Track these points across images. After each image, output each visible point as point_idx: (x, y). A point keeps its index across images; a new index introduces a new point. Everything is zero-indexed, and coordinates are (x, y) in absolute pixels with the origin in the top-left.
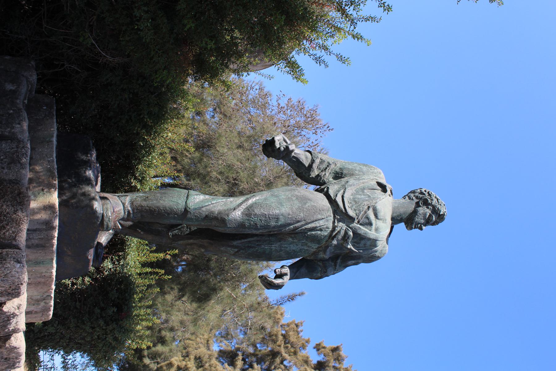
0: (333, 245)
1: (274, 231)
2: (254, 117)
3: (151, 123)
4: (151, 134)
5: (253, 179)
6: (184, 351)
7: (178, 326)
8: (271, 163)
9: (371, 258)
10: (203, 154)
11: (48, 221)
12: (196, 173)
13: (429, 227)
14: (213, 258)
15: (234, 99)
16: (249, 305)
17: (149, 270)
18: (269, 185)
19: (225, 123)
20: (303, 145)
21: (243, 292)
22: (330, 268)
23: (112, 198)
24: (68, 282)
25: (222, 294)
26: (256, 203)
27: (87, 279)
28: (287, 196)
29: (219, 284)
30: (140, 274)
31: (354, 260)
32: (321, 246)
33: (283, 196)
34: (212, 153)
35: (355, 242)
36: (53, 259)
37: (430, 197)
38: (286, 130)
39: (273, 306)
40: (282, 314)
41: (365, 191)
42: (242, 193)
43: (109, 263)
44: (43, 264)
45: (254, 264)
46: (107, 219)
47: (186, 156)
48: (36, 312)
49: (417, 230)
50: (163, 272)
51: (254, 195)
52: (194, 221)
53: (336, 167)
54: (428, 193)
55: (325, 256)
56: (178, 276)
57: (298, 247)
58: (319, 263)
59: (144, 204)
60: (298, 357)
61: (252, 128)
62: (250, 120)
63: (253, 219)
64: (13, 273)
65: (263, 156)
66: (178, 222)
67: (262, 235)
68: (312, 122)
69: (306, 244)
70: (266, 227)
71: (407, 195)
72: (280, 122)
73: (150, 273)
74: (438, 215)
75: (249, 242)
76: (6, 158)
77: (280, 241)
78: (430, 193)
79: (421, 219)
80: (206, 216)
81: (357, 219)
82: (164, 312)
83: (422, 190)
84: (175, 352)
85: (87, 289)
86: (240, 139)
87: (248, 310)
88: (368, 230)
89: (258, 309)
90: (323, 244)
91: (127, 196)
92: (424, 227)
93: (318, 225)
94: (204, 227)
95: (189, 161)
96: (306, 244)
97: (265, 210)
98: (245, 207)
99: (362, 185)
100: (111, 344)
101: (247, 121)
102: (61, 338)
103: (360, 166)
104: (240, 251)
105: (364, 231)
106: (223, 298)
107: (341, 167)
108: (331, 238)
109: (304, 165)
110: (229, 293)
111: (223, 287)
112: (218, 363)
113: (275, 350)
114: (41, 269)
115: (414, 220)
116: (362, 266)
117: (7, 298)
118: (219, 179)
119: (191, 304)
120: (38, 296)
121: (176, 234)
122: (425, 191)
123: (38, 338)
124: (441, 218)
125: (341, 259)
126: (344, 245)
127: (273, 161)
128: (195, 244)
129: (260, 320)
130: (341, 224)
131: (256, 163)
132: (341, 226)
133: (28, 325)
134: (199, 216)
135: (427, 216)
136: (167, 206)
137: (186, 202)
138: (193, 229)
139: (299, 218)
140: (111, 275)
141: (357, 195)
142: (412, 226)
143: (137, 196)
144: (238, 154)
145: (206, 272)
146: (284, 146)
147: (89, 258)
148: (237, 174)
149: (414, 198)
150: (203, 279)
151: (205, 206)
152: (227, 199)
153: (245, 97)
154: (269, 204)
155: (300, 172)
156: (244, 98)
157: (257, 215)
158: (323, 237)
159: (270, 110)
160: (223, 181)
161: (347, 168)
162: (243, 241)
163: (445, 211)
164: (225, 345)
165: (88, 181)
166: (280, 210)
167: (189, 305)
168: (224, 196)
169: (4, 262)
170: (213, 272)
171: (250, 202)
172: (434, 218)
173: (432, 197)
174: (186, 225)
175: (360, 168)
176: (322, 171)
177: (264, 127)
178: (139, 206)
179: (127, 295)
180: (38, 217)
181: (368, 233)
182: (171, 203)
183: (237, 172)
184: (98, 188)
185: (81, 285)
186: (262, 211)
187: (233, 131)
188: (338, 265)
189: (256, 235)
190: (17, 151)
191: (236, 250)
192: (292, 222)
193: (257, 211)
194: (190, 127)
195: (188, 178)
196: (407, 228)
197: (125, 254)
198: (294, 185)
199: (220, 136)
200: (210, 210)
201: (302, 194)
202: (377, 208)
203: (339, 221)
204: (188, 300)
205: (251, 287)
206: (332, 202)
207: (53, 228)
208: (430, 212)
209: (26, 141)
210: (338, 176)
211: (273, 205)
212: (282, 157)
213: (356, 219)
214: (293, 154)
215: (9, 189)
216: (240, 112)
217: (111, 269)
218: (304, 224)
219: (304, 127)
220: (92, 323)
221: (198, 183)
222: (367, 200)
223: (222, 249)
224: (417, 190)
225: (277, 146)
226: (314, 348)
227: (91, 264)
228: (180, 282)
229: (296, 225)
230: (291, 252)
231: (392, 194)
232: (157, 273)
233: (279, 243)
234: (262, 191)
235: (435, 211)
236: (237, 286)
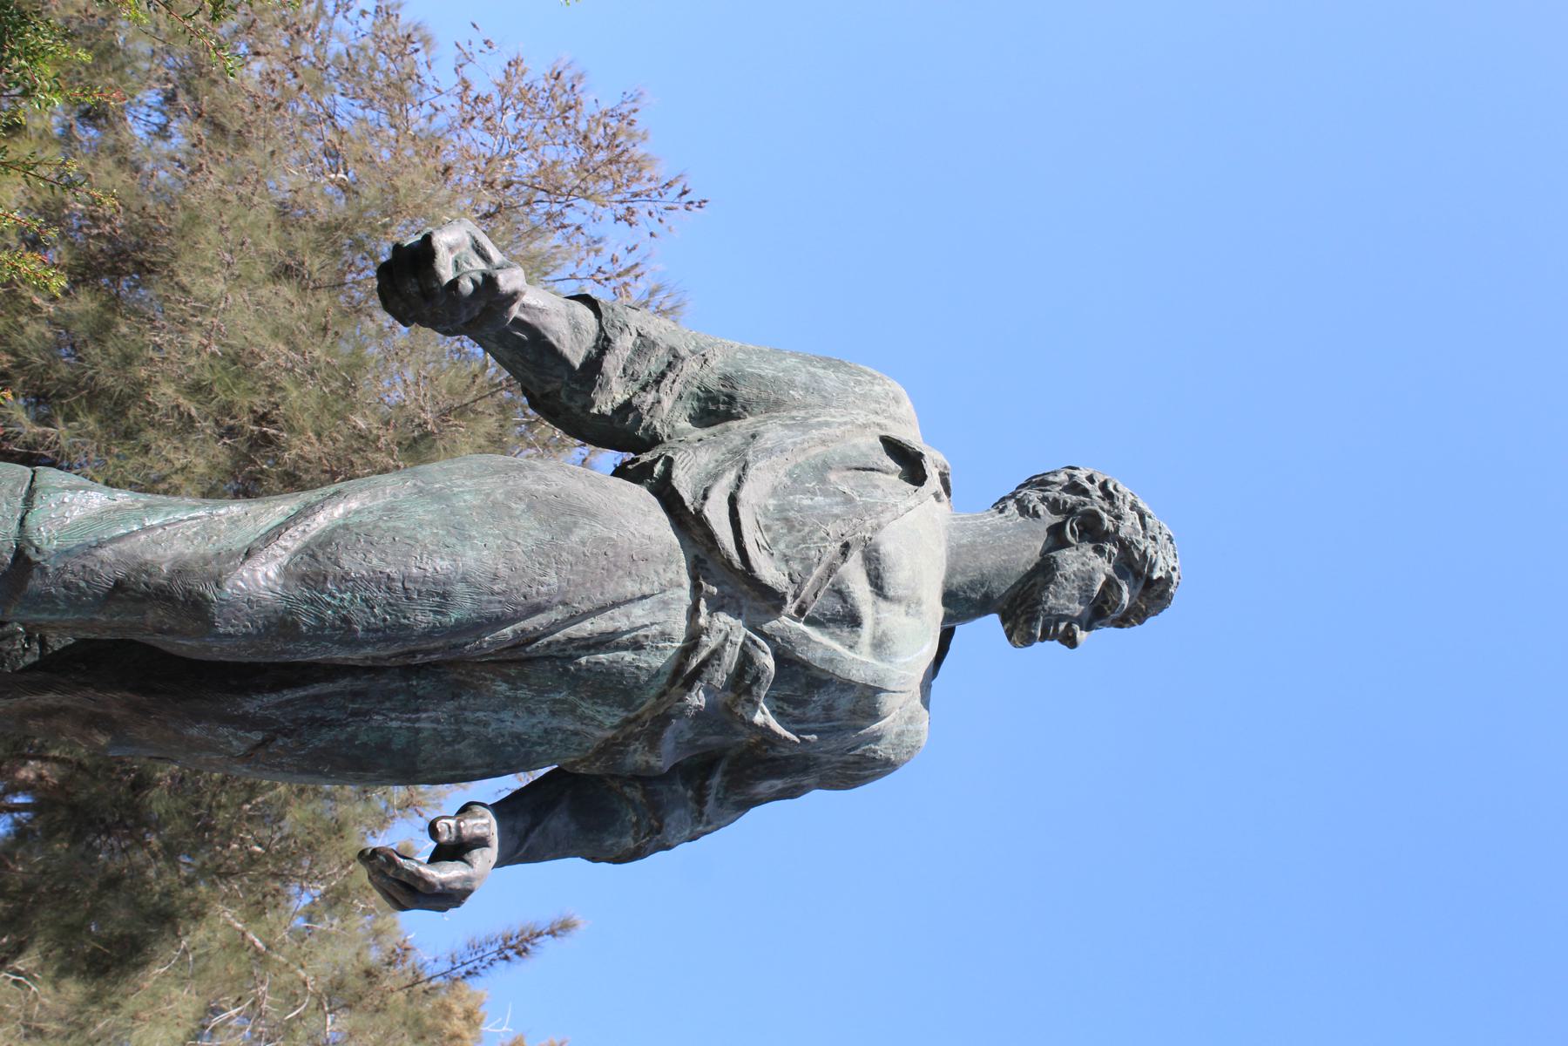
0: (690, 713)
1: (428, 652)
2: (351, 141)
5: (345, 419)
8: (429, 349)
10: (113, 304)
12: (80, 390)
14: (158, 775)
15: (257, 54)
16: (325, 980)
19: (217, 162)
20: (570, 268)
21: (300, 922)
22: (679, 813)
25: (201, 934)
26: (346, 527)
28: (488, 495)
29: (187, 893)
31: (780, 774)
32: (638, 717)
33: (467, 497)
34: (158, 296)
35: (785, 699)
37: (1112, 504)
38: (498, 199)
39: (433, 983)
40: (469, 1016)
41: (833, 477)
42: (292, 481)
45: (349, 798)
47: (35, 308)
49: (1055, 646)
52: (62, 606)
53: (706, 370)
54: (1104, 486)
55: (653, 761)
57: (535, 721)
58: (627, 790)
61: (344, 188)
62: (331, 153)
63: (334, 597)
67: (373, 669)
68: (614, 168)
69: (573, 710)
70: (394, 632)
71: (1013, 495)
72: (470, 164)
74: (1142, 583)
75: (318, 698)
77: (455, 696)
78: (1111, 487)
79: (1070, 599)
80: (119, 585)
81: (796, 596)
83: (1076, 472)
86: (284, 235)
87: (320, 1006)
88: (843, 644)
89: (367, 1001)
90: (642, 709)
92: (1081, 636)
93: (623, 624)
94: (107, 636)
95: (49, 335)
96: (573, 710)
97: (389, 559)
101: (321, 156)
103: (812, 369)
104: (273, 740)
105: (827, 648)
106: (207, 954)
107: (730, 370)
108: (680, 681)
109: (563, 360)
110: (236, 929)
111: (204, 903)
115: (1039, 602)
116: (817, 799)
118: (189, 415)
119: (57, 988)
122: (1091, 479)
125: (725, 774)
126: (739, 710)
127: (433, 343)
130: (724, 620)
131: (363, 347)
132: (724, 629)
134: (83, 584)
135: (1098, 588)
137: (23, 519)
138: (57, 643)
139: (538, 594)
142: (1030, 627)
144: (279, 304)
145: (130, 836)
146: (474, 275)
148: (270, 394)
149: (1042, 508)
151: (113, 540)
152: (215, 507)
153: (311, 48)
154: (408, 533)
155: (548, 388)
156: (305, 50)
157: (353, 580)
158: (644, 678)
159: (426, 109)
160: (208, 426)
161: (752, 374)
162: (288, 694)
163: (1172, 563)
166: (454, 557)
167: (49, 989)
168: (211, 493)
170: (159, 837)
171: (321, 521)
172: (1126, 597)
173: (1119, 503)
174: (23, 625)
175: (813, 375)
176: (643, 389)
177: (398, 183)
183: (273, 388)
186: (375, 561)
187: (256, 199)
188: (711, 800)
189: (333, 671)
191: (257, 736)
192: (509, 610)
193: (352, 563)
194: (43, 179)
195: (43, 410)
196: (1009, 638)
198: (530, 445)
199: (194, 219)
200: (135, 557)
201: (554, 489)
202: (882, 549)
203: (716, 606)
204: (42, 969)
205: (336, 899)
208: (1109, 568)
211: (425, 534)
212: (466, 324)
213: (789, 599)
214: (515, 311)
216: (288, 116)
218: (563, 621)
219: (576, 191)
221: (92, 435)
222: (837, 516)
223: (194, 732)
224: (1055, 473)
225: (442, 271)
229: (529, 624)
230: (505, 744)
233: (451, 705)
234: (385, 470)
235: (1130, 566)
236: (269, 899)
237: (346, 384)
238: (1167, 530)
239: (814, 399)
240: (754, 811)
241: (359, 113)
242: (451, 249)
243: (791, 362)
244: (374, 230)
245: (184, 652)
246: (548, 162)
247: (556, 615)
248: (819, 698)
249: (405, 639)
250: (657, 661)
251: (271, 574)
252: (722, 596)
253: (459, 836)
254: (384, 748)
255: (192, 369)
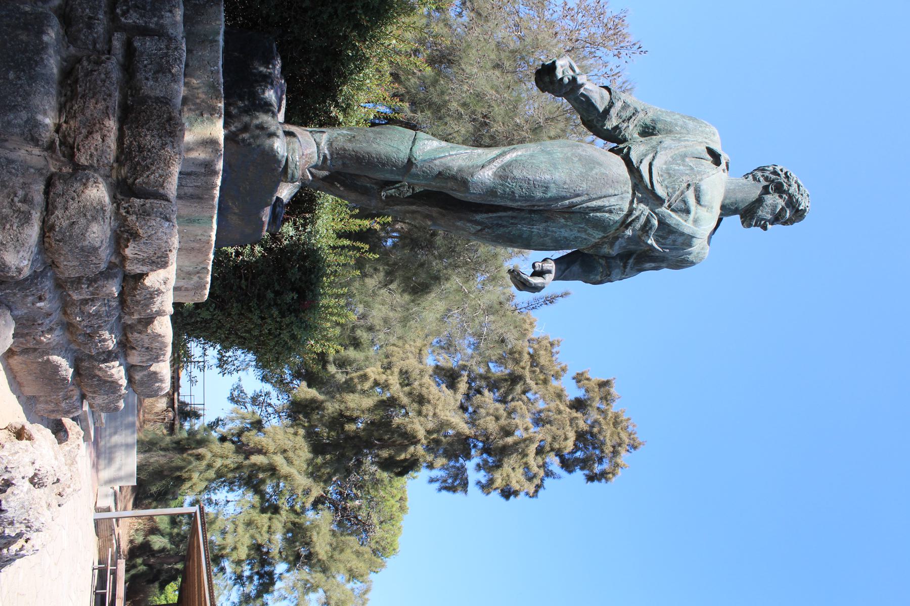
1: (539, 206)
3: (368, 22)
4: (365, 40)
5: (513, 119)
6: (385, 360)
7: (380, 325)
9: (681, 263)
10: (439, 73)
11: (209, 162)
12: (426, 102)
13: (778, 227)
17: (347, 242)
18: (536, 131)
22: (617, 270)
23: (301, 134)
24: (231, 250)
25: (448, 285)
27: (257, 248)
30: (334, 248)
31: (654, 262)
35: (660, 236)
36: (212, 217)
37: (788, 180)
40: (531, 324)
41: (687, 160)
42: (493, 143)
43: (291, 229)
44: (199, 223)
46: (293, 166)
47: (414, 73)
48: (187, 289)
49: (759, 229)
50: (367, 247)
51: (514, 148)
53: (646, 117)
54: (786, 173)
55: (611, 251)
56: (386, 253)
59: (349, 146)
60: (549, 388)
61: (520, 38)
62: (517, 25)
64: (160, 234)
65: (531, 84)
66: (397, 177)
67: (520, 210)
68: (615, 37)
69: (585, 231)
70: (528, 198)
71: (751, 173)
73: (348, 247)
75: (500, 217)
76: (151, 64)
77: (546, 222)
78: (788, 174)
79: (767, 213)
80: (440, 173)
81: (668, 201)
82: (361, 303)
84: (373, 361)
85: (256, 262)
91: (324, 132)
92: (769, 226)
93: (607, 204)
96: (585, 231)
98: (500, 165)
99: (684, 149)
100: (286, 343)
102: (219, 328)
105: (677, 220)
112: (432, 383)
113: (517, 373)
114: (196, 229)
115: (756, 213)
116: (666, 272)
117: (150, 267)
120: (190, 266)
121: (391, 195)
122: (781, 170)
123: (188, 324)
124: (798, 214)
126: (643, 238)
128: (418, 212)
129: (501, 327)
130: (642, 206)
132: (642, 210)
133: (176, 305)
135: (778, 210)
136: (382, 152)
138: (417, 190)
140: (291, 245)
141: (673, 164)
143: (338, 134)
147: (264, 219)
149: (762, 179)
150: (422, 261)
155: (590, 118)
158: (611, 223)
159: (551, 11)
160: (466, 118)
162: (491, 215)
164: (448, 362)
165: (266, 107)
168: (464, 142)
169: (148, 217)
172: (788, 214)
173: (791, 180)
175: (684, 122)
176: (623, 121)
178: (341, 149)
179: (313, 276)
180: (194, 155)
181: (682, 225)
182: (389, 149)
183: (490, 106)
184: (281, 117)
185: (249, 255)
188: (629, 267)
189: (506, 209)
190: (166, 55)
191: (479, 228)
192: (568, 195)
193: (517, 173)
196: (743, 224)
197: (313, 216)
198: (575, 133)
201: (588, 154)
202: (702, 188)
203: (640, 201)
205: (493, 279)
206: (633, 170)
207: (215, 173)
208: (783, 204)
209: (180, 39)
210: (648, 131)
211: (543, 166)
214: (582, 90)
215: (155, 111)
217: (292, 236)
220: (261, 312)
223: (459, 224)
224: (768, 167)
226: (574, 378)
227: (266, 228)
228: (388, 261)
229: (574, 200)
231: (728, 169)
232: (359, 249)
233: (544, 225)
237: (515, 107)
238: (807, 192)
239: (684, 131)
240: (642, 273)
241: (528, 11)
242: (562, 67)
243: (677, 116)
244: (529, 53)
245: (459, 197)
246: (592, 32)
247: (583, 198)
248: (672, 237)
249: (531, 201)
250: (617, 218)
251: (490, 174)
252: (642, 198)
253: (542, 269)
254: (520, 236)
255: (463, 98)
